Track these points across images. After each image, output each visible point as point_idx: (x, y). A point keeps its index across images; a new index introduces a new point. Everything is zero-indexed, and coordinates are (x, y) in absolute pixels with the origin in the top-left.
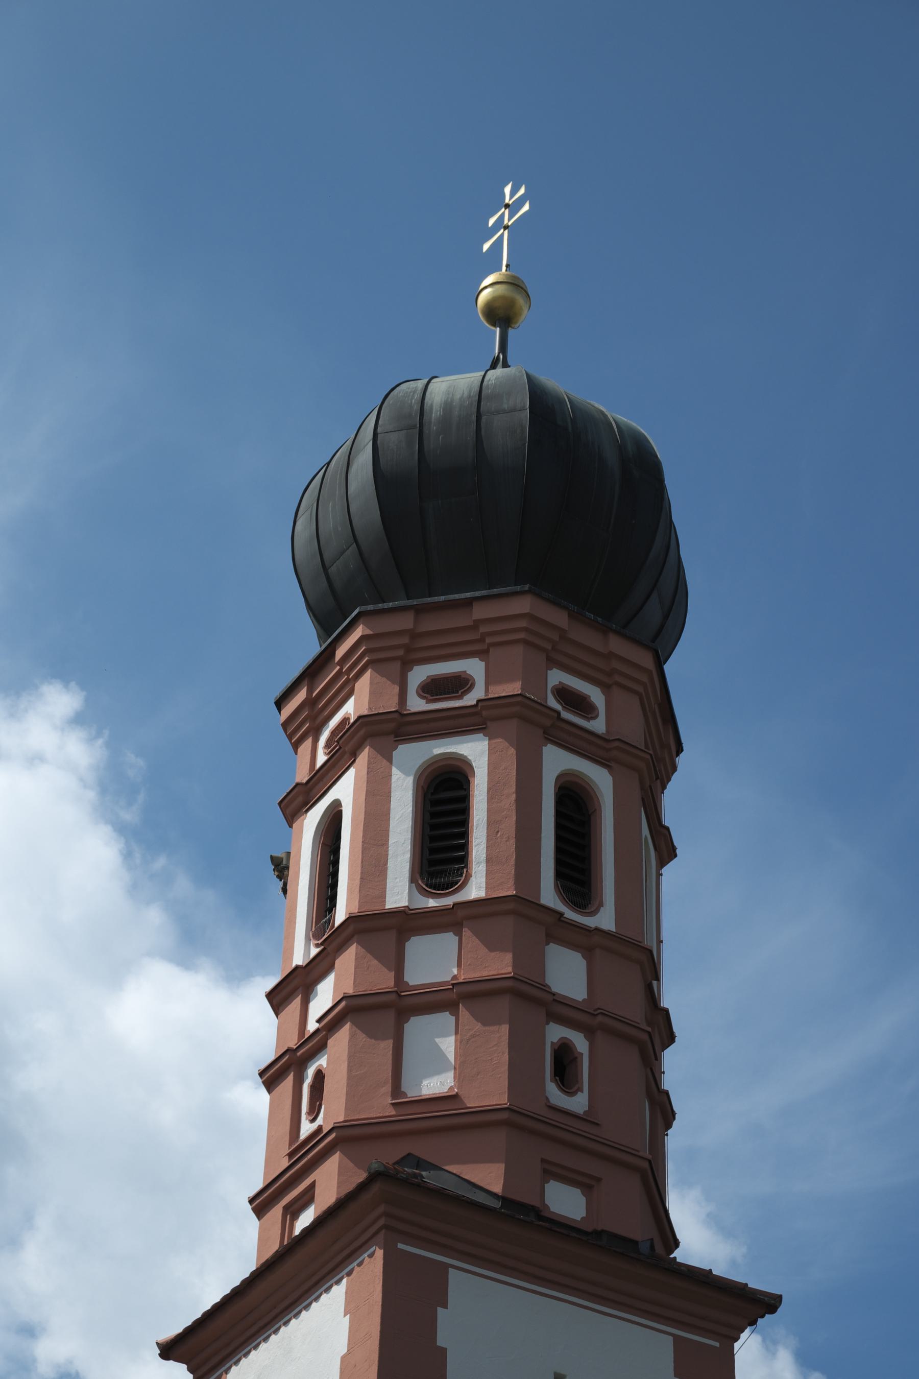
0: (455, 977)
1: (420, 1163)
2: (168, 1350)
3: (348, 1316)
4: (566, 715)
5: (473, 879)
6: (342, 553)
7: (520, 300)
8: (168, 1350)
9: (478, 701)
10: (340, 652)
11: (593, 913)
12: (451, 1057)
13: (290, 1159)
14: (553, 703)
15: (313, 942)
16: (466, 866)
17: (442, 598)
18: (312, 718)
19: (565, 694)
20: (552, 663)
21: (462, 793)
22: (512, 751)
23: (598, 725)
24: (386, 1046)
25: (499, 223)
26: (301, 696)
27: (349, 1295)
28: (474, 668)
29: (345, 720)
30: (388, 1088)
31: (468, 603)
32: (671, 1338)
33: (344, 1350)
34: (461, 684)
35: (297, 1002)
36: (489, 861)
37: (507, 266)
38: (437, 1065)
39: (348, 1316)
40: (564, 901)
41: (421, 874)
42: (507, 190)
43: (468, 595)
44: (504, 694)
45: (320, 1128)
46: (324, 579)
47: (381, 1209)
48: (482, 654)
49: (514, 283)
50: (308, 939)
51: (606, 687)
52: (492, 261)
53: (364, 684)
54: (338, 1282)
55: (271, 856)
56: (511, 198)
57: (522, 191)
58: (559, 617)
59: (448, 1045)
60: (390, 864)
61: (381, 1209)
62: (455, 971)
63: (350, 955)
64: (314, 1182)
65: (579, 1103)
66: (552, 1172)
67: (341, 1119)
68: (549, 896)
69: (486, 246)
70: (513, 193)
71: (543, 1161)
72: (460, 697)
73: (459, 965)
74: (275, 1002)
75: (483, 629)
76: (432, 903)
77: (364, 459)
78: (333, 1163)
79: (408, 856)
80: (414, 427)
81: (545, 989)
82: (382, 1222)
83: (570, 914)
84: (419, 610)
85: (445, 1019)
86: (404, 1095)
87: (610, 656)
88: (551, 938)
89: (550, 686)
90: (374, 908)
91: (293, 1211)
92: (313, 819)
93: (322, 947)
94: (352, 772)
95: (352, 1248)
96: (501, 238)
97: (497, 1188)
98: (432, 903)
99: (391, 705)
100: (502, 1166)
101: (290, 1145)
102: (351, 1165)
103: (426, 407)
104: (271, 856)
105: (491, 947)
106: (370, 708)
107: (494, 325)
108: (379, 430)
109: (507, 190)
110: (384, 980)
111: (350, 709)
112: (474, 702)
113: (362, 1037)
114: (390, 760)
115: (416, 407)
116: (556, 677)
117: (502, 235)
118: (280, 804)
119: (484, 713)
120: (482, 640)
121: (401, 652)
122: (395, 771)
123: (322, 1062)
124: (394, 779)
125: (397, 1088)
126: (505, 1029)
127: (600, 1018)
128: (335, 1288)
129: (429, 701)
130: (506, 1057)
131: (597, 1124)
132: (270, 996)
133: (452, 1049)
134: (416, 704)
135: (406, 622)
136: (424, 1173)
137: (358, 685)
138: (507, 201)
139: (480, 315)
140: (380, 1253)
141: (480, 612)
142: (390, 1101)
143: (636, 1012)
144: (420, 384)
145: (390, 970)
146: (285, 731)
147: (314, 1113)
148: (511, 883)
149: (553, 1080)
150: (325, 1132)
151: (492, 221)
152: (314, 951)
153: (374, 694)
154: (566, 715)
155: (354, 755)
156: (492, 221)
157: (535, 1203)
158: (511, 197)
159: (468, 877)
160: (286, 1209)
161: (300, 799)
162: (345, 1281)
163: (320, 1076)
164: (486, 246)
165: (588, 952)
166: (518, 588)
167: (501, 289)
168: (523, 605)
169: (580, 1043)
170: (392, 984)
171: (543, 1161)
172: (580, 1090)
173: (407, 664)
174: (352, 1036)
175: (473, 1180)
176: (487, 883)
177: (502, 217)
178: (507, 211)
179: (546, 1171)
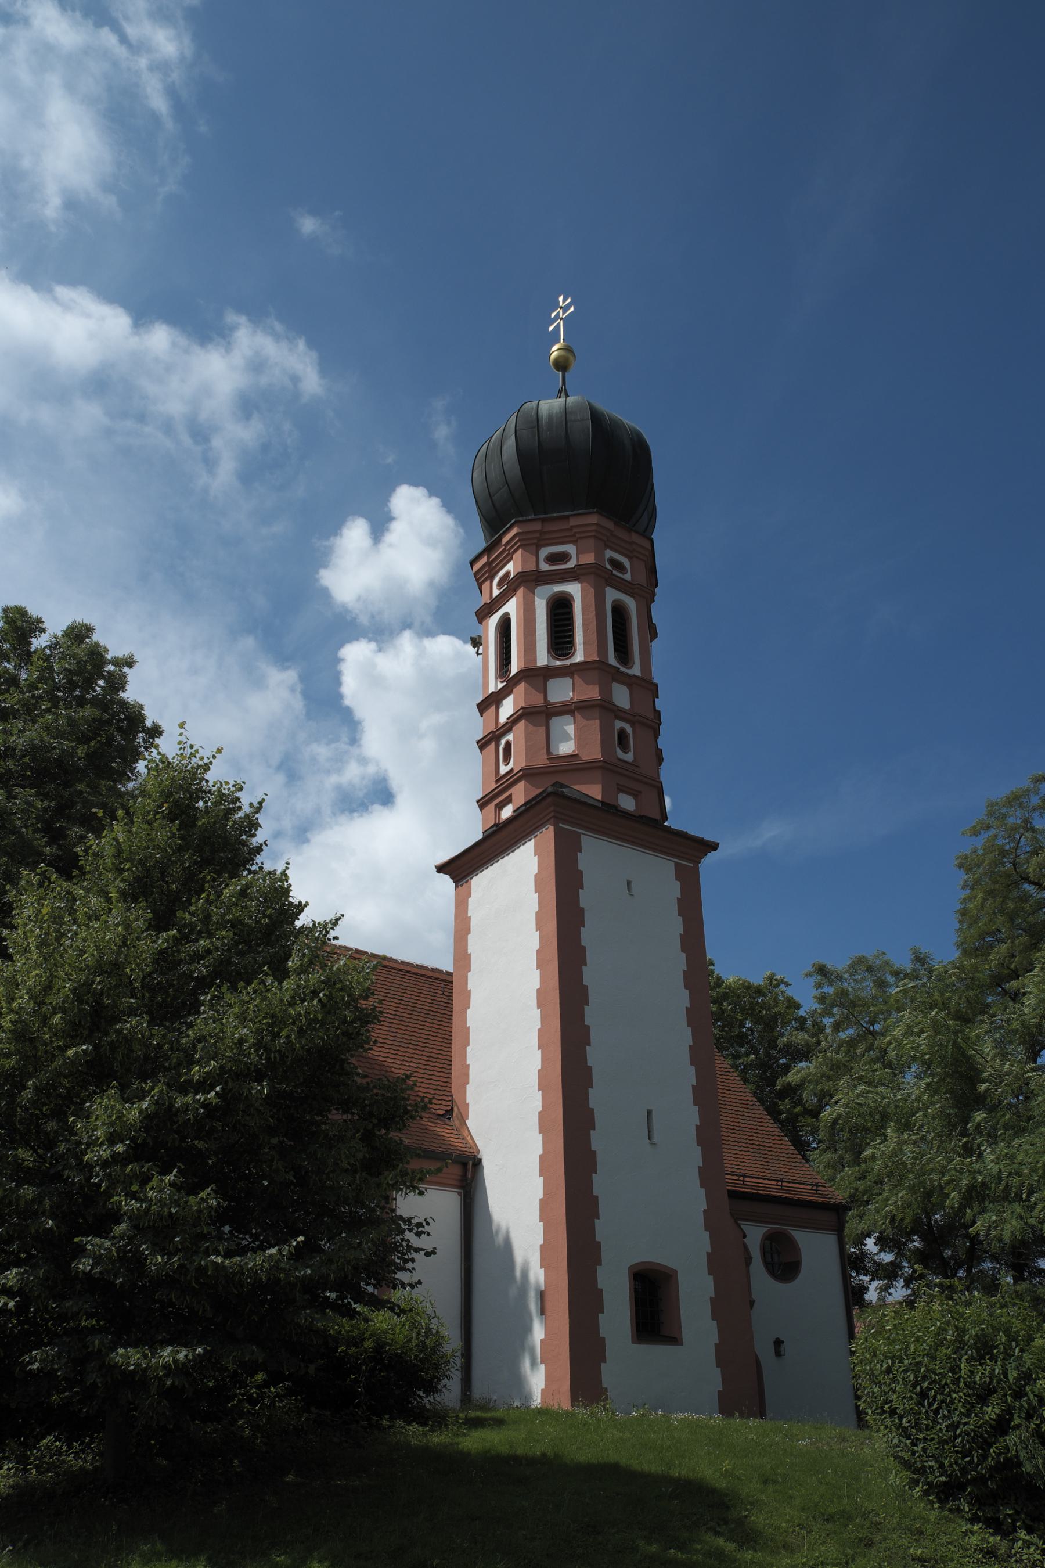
0: (572, 699)
1: (563, 786)
2: (441, 869)
3: (255, 841)
4: (615, 572)
5: (577, 652)
6: (501, 489)
7: (571, 358)
8: (441, 869)
9: (575, 566)
10: (505, 540)
11: (631, 668)
12: (573, 737)
13: (496, 783)
14: (608, 566)
15: (498, 680)
16: (574, 645)
17: (555, 515)
18: (489, 571)
19: (613, 562)
20: (607, 547)
21: (568, 610)
22: (593, 590)
23: (628, 577)
24: (542, 730)
25: (557, 316)
26: (484, 560)
27: (536, 845)
28: (571, 549)
29: (508, 573)
30: (545, 751)
31: (567, 517)
32: (673, 863)
33: (536, 872)
34: (564, 557)
35: (493, 708)
36: (584, 643)
37: (563, 339)
38: (566, 738)
39: (255, 841)
40: (619, 662)
41: (552, 648)
42: (561, 299)
43: (567, 513)
44: (587, 563)
45: (512, 770)
46: (490, 501)
47: (552, 809)
48: (574, 542)
49: (568, 349)
50: (496, 678)
51: (630, 558)
52: (554, 337)
53: (518, 555)
54: (530, 840)
55: (471, 638)
56: (563, 303)
57: (569, 300)
58: (609, 524)
59: (570, 729)
60: (538, 644)
61: (552, 809)
62: (571, 694)
63: (521, 688)
64: (511, 795)
65: (629, 757)
66: (622, 789)
67: (524, 765)
68: (612, 660)
69: (551, 328)
70: (564, 301)
71: (617, 784)
72: (565, 563)
73: (573, 691)
74: (481, 708)
75: (575, 530)
76: (558, 663)
77: (510, 443)
78: (521, 786)
79: (546, 640)
80: (535, 427)
81: (613, 704)
82: (552, 814)
83: (622, 669)
84: (543, 520)
85: (569, 718)
86: (552, 754)
87: (572, 527)
88: (614, 680)
89: (606, 558)
90: (531, 666)
91: (500, 807)
92: (493, 621)
93: (505, 683)
94: (514, 600)
95: (536, 825)
96: (559, 324)
97: (599, 797)
98: (558, 663)
99: (532, 567)
100: (600, 786)
101: (496, 777)
102: (530, 786)
103: (540, 417)
104: (471, 638)
105: (588, 683)
106: (522, 569)
107: (559, 370)
108: (517, 428)
109: (561, 299)
110: (538, 700)
111: (510, 567)
112: (573, 566)
113: (530, 726)
114: (534, 594)
115: (535, 417)
116: (609, 553)
117: (559, 323)
118: (476, 613)
119: (578, 572)
120: (574, 535)
121: (536, 541)
122: (536, 598)
123: (510, 737)
124: (536, 603)
125: (549, 752)
126: (598, 722)
127: (637, 717)
128: (528, 844)
129: (550, 565)
130: (599, 737)
131: (638, 767)
132: (479, 705)
133: (573, 733)
134: (545, 567)
135: (537, 526)
136: (564, 790)
137: (514, 556)
138: (561, 304)
139: (552, 367)
140: (551, 828)
141: (573, 522)
142: (546, 757)
143: (651, 715)
144: (535, 403)
145: (540, 693)
146: (475, 577)
147: (507, 760)
148: (596, 654)
149: (619, 747)
150: (515, 773)
151: (553, 315)
152: (500, 685)
153: (524, 561)
154: (615, 572)
155: (515, 591)
156: (553, 315)
157: (616, 804)
158: (563, 302)
159: (575, 650)
160: (496, 805)
161: (486, 611)
162: (533, 840)
163: (508, 744)
164: (551, 328)
165: (629, 686)
166: (591, 510)
167: (562, 352)
168: (594, 519)
169: (629, 729)
170: (543, 701)
171: (617, 784)
172: (630, 751)
173: (538, 547)
174: (526, 727)
175: (587, 794)
176: (584, 654)
177: (559, 313)
178: (561, 311)
179: (618, 789)
